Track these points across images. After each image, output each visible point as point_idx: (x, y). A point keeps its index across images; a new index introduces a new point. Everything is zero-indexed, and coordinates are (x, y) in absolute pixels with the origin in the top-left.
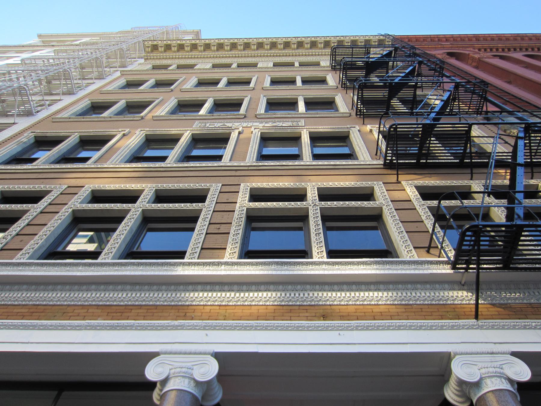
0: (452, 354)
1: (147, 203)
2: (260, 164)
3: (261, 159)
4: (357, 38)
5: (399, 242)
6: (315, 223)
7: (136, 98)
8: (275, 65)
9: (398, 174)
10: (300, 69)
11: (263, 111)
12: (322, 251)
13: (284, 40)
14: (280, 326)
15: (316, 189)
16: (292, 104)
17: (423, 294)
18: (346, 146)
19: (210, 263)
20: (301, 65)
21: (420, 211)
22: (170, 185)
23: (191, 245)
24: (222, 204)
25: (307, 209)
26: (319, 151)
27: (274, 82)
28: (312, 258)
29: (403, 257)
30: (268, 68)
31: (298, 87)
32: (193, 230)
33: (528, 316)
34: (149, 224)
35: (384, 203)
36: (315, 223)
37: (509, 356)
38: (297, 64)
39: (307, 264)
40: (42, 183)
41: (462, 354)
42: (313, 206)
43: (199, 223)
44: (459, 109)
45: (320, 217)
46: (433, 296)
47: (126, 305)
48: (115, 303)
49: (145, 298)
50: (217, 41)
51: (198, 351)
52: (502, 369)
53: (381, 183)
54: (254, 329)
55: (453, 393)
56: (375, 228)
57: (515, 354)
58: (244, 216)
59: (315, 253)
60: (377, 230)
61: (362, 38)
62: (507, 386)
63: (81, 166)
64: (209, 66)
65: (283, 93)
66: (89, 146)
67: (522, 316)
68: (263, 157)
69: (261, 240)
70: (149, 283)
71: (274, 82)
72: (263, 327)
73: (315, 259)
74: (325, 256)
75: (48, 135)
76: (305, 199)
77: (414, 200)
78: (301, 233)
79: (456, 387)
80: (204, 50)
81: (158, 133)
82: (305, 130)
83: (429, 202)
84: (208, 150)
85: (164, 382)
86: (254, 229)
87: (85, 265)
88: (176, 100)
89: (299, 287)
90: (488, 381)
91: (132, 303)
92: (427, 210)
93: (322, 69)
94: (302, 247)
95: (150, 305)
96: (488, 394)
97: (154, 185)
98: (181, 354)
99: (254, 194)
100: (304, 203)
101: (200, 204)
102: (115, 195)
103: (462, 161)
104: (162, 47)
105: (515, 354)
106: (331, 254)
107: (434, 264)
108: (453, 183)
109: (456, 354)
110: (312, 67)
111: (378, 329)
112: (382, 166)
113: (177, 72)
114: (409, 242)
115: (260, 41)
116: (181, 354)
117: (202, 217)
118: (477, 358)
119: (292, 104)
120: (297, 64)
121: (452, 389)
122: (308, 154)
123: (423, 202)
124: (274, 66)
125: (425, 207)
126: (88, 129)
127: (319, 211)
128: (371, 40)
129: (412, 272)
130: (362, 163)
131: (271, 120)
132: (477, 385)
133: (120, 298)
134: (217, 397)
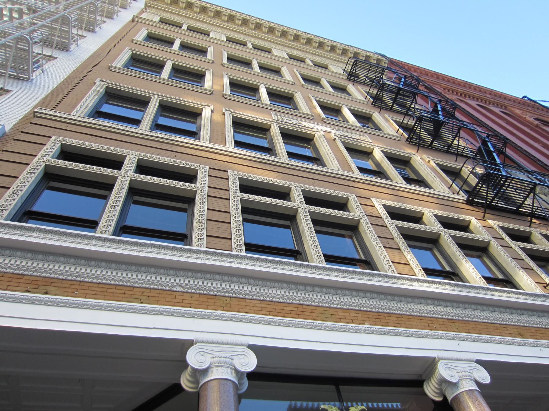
0: (437, 359)
1: (52, 157)
2: (154, 134)
3: (97, 115)
4: (263, 22)
5: (310, 246)
6: (118, 195)
7: (184, 62)
8: (162, 21)
9: (485, 213)
10: (253, 52)
11: (120, 65)
12: (203, 239)
13: (355, 50)
14: (132, 309)
15: (237, 179)
16: (158, 66)
17: (319, 297)
18: (266, 139)
19: (438, 282)
20: (190, 29)
21: (391, 229)
22: (262, 178)
23: (105, 216)
24: (17, 155)
25: (195, 192)
26: (163, 121)
27: (151, 37)
28: (190, 245)
29: (313, 262)
30: (154, 22)
31: (173, 50)
32: (105, 198)
33: (470, 331)
34: (51, 182)
35: (300, 205)
36: (118, 195)
37: (246, 347)
38: (185, 27)
39: (185, 250)
40: (175, 157)
41: (202, 342)
42: (125, 176)
43: (114, 192)
44: (458, 149)
45: (240, 208)
46: (228, 289)
47: (378, 312)
48: (87, 280)
49: (80, 273)
50: (228, 11)
51: (220, 341)
52: (232, 359)
53: (355, 196)
54: (43, 303)
55: (432, 390)
56: (287, 227)
57: (478, 362)
58: (126, 187)
59: (194, 240)
60: (290, 229)
61: (214, 7)
62: (231, 376)
63: (179, 139)
64: (157, 19)
65: (154, 52)
66: (298, 142)
67: (294, 316)
68: (97, 113)
69: (142, 216)
70: (76, 257)
71: (151, 37)
72: (191, 315)
73: (234, 252)
74: (244, 249)
75: (122, 88)
76: (194, 182)
77: (384, 218)
78: (185, 215)
79: (436, 385)
80: (185, 8)
81: (244, 117)
82: (156, 96)
83: (310, 207)
84: (294, 147)
85: (205, 372)
86: (136, 202)
87: (339, 271)
88: (130, 53)
89: (208, 276)
90: (464, 382)
91: (20, 272)
92: (308, 214)
93: (273, 57)
94: (183, 231)
95: (127, 286)
96: (212, 382)
97: (137, 153)
98: (221, 345)
99: (141, 164)
100: (193, 185)
101: (116, 171)
102: (404, 214)
103: (518, 209)
104: (212, 11)
105: (478, 362)
106: (250, 247)
107: (431, 283)
108: (286, 183)
109: (440, 359)
110: (239, 45)
111: (172, 315)
112: (464, 202)
113: (158, 25)
114: (319, 248)
115: (334, 44)
116: (221, 345)
117: (117, 185)
118: (217, 348)
119: (158, 66)
120: (185, 27)
121: (433, 388)
122: (147, 121)
123: (305, 206)
124: (188, 29)
125: (307, 210)
126: (138, 87)
127: (239, 202)
128: (313, 39)
129: (279, 271)
130: (330, 171)
131: (358, 133)
132: (205, 372)
133: (50, 269)
134: (241, 389)
